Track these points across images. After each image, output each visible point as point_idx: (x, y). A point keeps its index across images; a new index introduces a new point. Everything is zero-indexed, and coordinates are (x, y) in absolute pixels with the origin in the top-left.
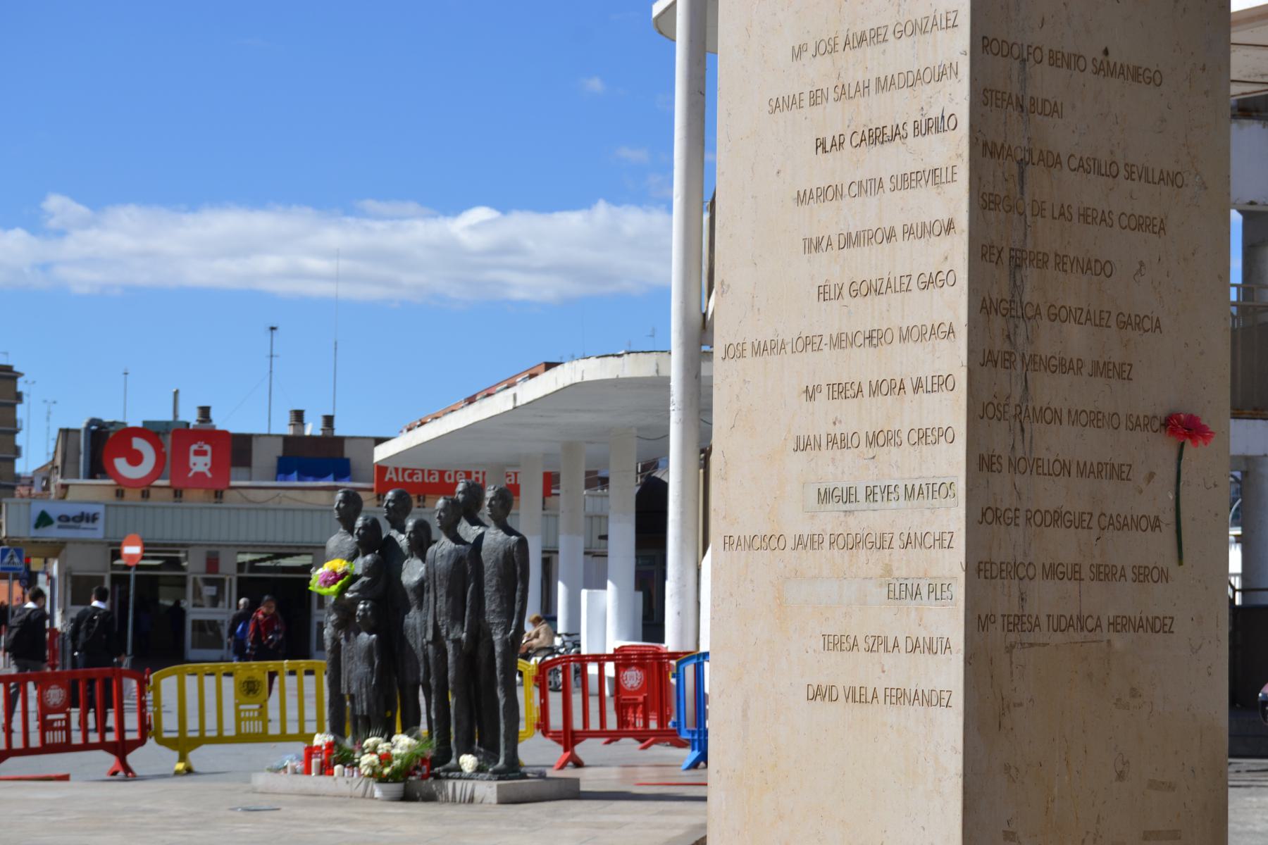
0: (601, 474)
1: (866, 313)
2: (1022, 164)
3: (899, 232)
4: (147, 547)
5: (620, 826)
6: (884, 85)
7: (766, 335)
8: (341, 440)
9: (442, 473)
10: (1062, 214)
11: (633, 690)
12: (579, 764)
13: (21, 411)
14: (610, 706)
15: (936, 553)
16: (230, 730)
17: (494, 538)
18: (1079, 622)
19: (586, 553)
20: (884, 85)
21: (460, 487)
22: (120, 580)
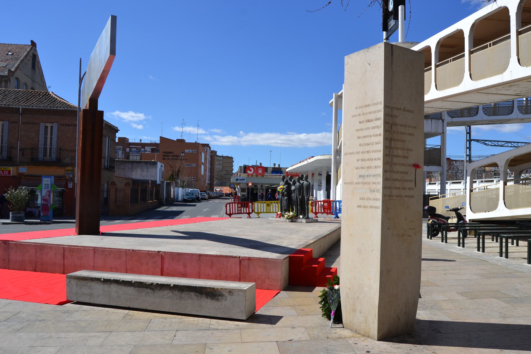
0: (320, 173)
1: (367, 148)
2: (392, 125)
3: (372, 135)
4: (252, 184)
5: (324, 227)
6: (370, 113)
7: (351, 151)
8: (281, 168)
9: (296, 173)
10: (398, 133)
12: (317, 217)
13: (234, 163)
14: (322, 208)
15: (378, 185)
17: (305, 183)
18: (400, 196)
19: (318, 185)
20: (370, 113)
21: (300, 175)
22: (248, 189)
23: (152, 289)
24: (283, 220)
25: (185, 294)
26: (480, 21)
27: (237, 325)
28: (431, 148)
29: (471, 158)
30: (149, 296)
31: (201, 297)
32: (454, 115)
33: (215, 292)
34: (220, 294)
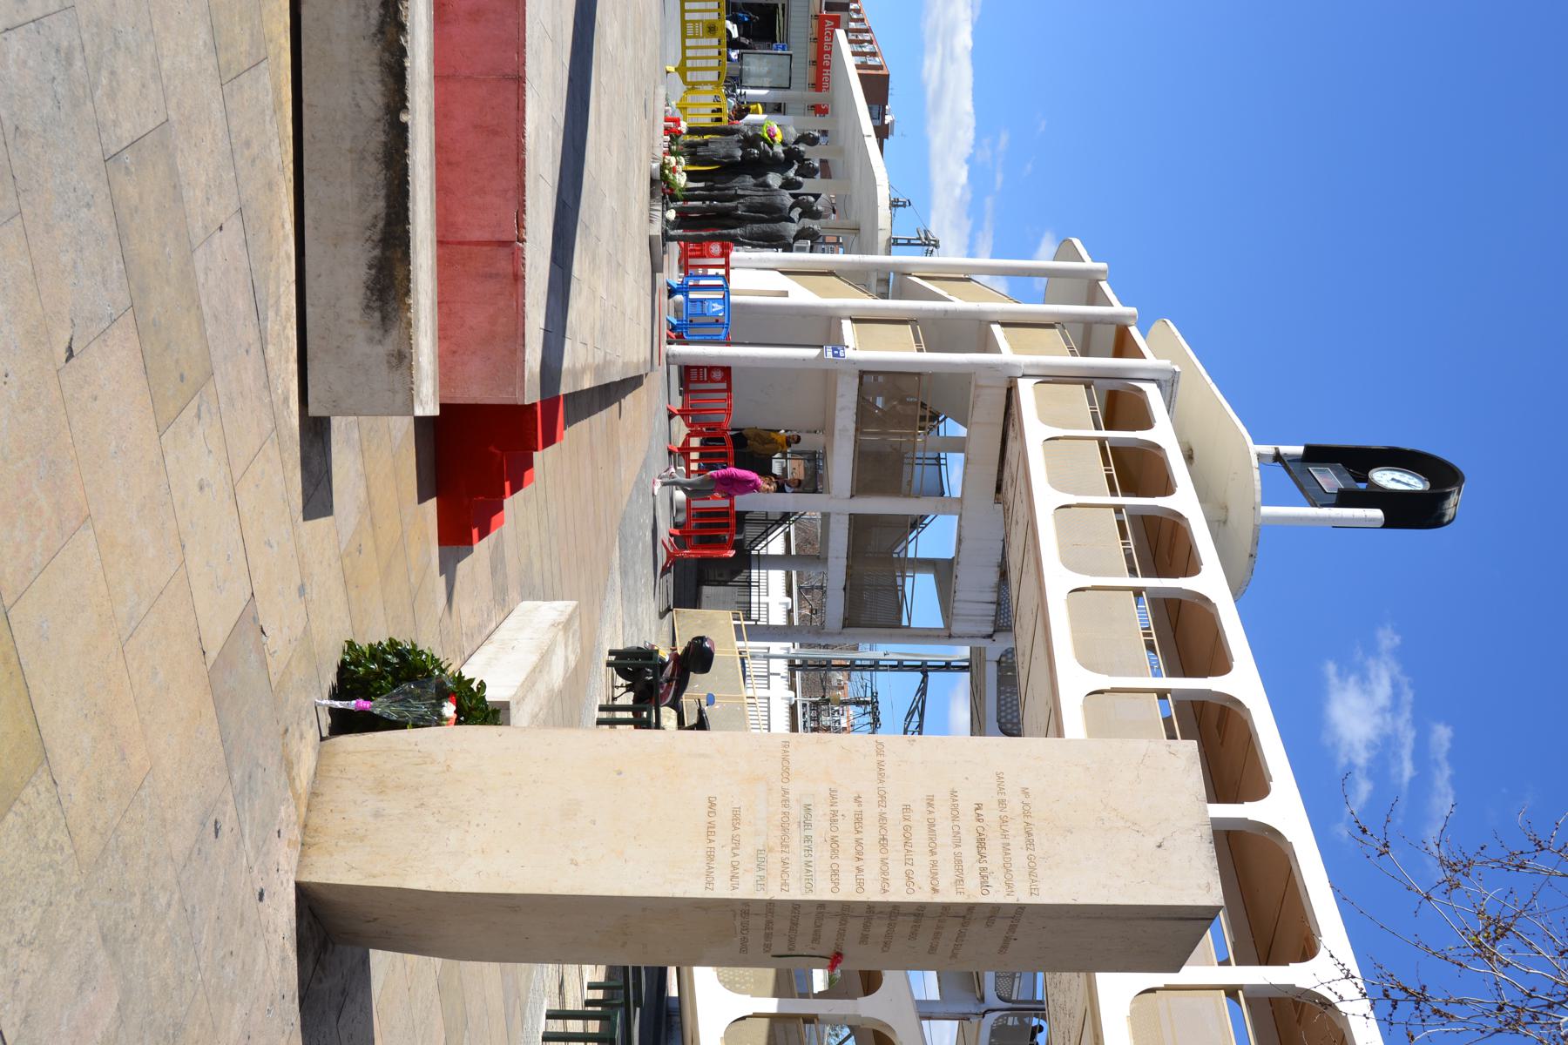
1: (895, 837)
3: (934, 858)
6: (1006, 847)
7: (888, 770)
9: (830, 52)
15: (779, 881)
20: (1006, 847)
23: (381, 30)
24: (657, 144)
25: (378, 174)
26: (1287, 855)
27: (286, 400)
28: (904, 596)
29: (871, 671)
30: (355, 16)
31: (373, 241)
32: (1005, 717)
33: (394, 298)
34: (390, 319)
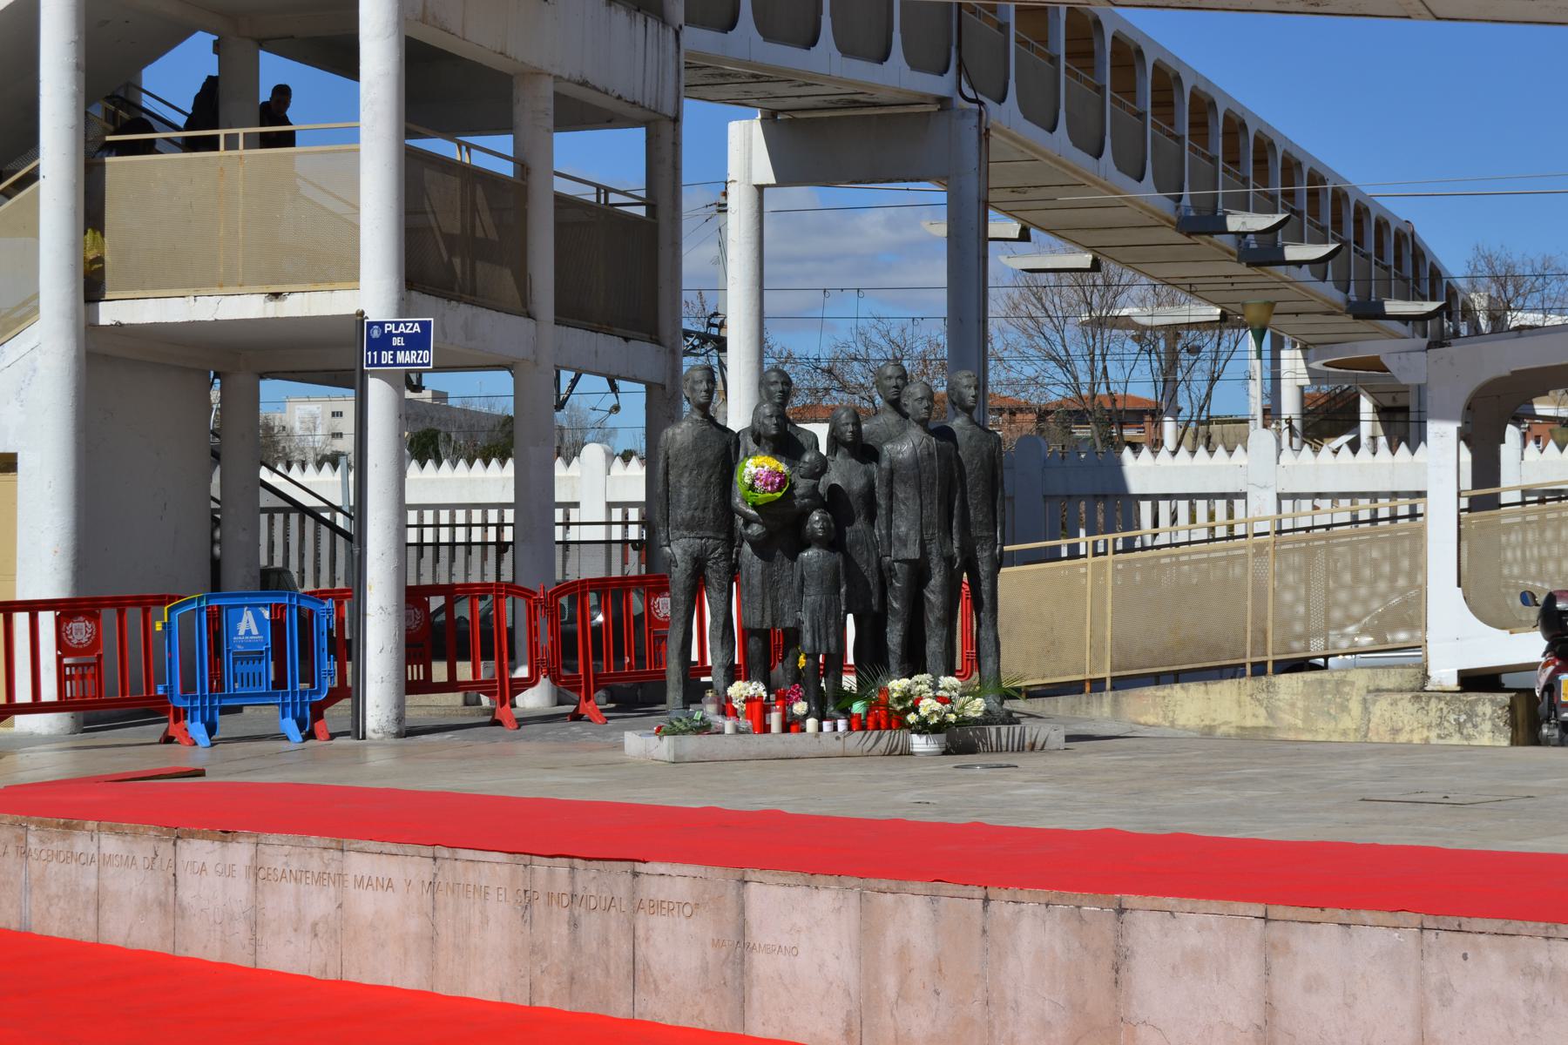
11: (81, 646)
16: (109, 616)
